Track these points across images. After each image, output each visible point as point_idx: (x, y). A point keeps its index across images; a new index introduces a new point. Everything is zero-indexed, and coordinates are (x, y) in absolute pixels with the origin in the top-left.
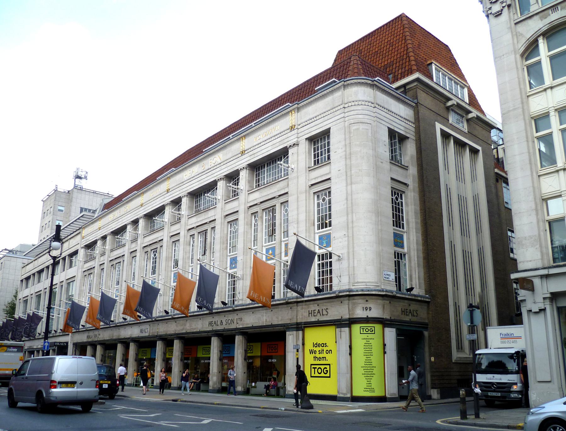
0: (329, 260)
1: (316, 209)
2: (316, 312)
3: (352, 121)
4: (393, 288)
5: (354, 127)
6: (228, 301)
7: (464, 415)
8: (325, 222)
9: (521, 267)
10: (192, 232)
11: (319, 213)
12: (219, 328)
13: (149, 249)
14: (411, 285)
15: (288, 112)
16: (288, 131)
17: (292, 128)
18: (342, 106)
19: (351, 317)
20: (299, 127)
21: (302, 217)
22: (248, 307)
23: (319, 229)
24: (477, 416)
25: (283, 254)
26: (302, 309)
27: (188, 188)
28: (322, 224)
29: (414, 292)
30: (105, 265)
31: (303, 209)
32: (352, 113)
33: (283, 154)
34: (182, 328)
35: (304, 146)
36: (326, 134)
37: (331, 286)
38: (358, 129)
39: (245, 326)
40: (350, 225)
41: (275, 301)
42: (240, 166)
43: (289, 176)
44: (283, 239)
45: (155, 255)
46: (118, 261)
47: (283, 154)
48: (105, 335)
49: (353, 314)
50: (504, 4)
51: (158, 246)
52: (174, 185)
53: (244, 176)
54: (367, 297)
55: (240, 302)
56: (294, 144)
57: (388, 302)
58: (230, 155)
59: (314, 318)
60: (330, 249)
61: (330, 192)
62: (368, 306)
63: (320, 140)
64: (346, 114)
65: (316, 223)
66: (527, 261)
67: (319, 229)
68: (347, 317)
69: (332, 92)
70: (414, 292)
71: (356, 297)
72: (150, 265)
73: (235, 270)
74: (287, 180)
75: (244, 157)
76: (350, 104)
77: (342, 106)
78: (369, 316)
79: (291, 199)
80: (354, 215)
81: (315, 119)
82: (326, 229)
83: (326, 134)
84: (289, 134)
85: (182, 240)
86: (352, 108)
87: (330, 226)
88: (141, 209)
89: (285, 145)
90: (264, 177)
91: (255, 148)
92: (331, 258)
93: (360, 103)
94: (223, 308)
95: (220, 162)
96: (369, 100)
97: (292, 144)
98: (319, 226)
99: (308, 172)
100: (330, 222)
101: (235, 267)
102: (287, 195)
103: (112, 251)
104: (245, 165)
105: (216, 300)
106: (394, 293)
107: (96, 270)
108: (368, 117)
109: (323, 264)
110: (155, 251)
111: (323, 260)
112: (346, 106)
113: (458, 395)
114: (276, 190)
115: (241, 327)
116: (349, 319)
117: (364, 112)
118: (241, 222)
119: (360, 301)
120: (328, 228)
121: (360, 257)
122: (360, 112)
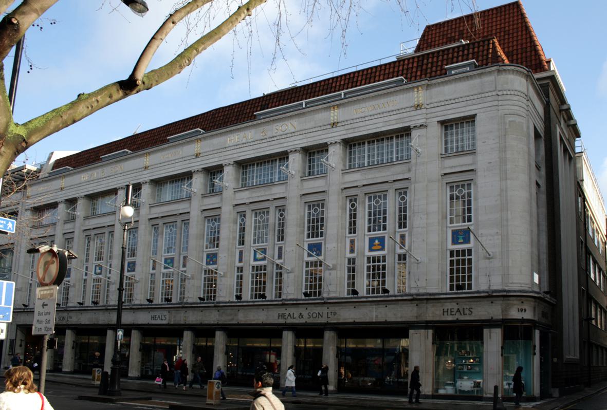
0: (467, 257)
1: (253, 225)
2: (157, 317)
3: (507, 112)
6: (125, 300)
15: (413, 88)
18: (494, 93)
19: (504, 317)
22: (199, 305)
23: (308, 237)
25: (181, 266)
26: (433, 306)
27: (235, 155)
32: (507, 102)
34: (230, 318)
37: (215, 296)
39: (341, 321)
41: (172, 304)
42: (196, 168)
43: (288, 181)
44: (182, 253)
52: (208, 150)
53: (229, 173)
54: (523, 299)
56: (296, 150)
57: (167, 312)
58: (309, 125)
59: (451, 316)
61: (219, 219)
62: (524, 307)
64: (500, 103)
67: (308, 237)
68: (501, 317)
71: (511, 298)
74: (285, 185)
75: (335, 129)
77: (494, 93)
78: (525, 318)
80: (509, 212)
81: (454, 101)
82: (317, 238)
86: (508, 97)
87: (217, 247)
88: (144, 172)
90: (253, 177)
91: (176, 161)
93: (516, 93)
94: (148, 305)
95: (120, 172)
97: (333, 142)
98: (309, 234)
99: (440, 159)
100: (218, 244)
101: (134, 270)
102: (113, 227)
104: (338, 139)
108: (522, 109)
109: (374, 266)
111: (257, 270)
112: (500, 93)
114: (388, 173)
115: (335, 321)
116: (502, 319)
117: (520, 104)
119: (515, 302)
120: (319, 238)
122: (517, 103)
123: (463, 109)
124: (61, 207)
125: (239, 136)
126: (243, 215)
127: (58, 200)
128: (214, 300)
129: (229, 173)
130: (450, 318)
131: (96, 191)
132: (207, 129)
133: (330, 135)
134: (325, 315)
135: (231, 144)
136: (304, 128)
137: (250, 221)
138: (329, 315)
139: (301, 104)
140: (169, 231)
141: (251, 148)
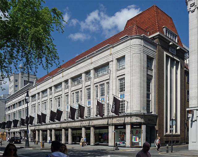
0: (124, 103)
4: (146, 112)
5: (134, 55)
7: (167, 152)
8: (122, 89)
9: (190, 106)
10: (73, 92)
11: (120, 87)
12: (85, 125)
13: (57, 98)
14: (152, 111)
16: (109, 56)
17: (111, 54)
18: (130, 47)
20: (113, 54)
21: (114, 88)
24: (172, 152)
28: (121, 90)
29: (153, 113)
30: (40, 103)
31: (114, 85)
33: (107, 64)
35: (115, 61)
36: (123, 58)
38: (135, 56)
40: (132, 91)
44: (107, 95)
45: (97, 89)
46: (45, 102)
47: (107, 64)
48: (43, 127)
49: (132, 121)
50: (196, 7)
51: (60, 97)
53: (92, 72)
55: (92, 117)
60: (124, 99)
63: (121, 59)
65: (119, 90)
66: (193, 105)
67: (120, 92)
69: (126, 41)
70: (153, 113)
72: (58, 104)
73: (90, 106)
76: (133, 46)
79: (111, 81)
80: (133, 88)
83: (123, 58)
84: (110, 57)
85: (69, 95)
87: (124, 91)
89: (108, 61)
92: (124, 102)
93: (137, 45)
96: (139, 44)
98: (120, 91)
100: (124, 90)
103: (42, 98)
104: (92, 68)
105: (84, 116)
106: (146, 114)
107: (36, 105)
110: (59, 98)
111: (123, 102)
113: (166, 146)
118: (92, 89)
121: (133, 104)
123: (122, 54)
124: (63, 84)
126: (97, 86)
127: (68, 78)
128: (124, 113)
129: (92, 72)
130: (118, 122)
132: (66, 67)
140: (88, 91)
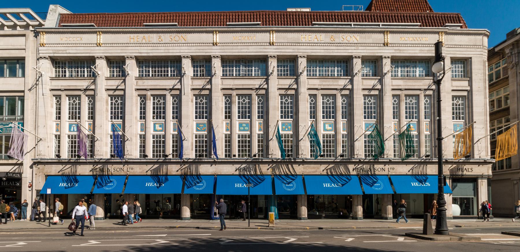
41: (147, 159)
104: (390, 55)
125: (138, 40)
131: (151, 54)
133: (383, 51)
134: (387, 170)
135: (304, 41)
136: (364, 42)
137: (66, 103)
138: (129, 169)
139: (379, 25)
141: (322, 48)
